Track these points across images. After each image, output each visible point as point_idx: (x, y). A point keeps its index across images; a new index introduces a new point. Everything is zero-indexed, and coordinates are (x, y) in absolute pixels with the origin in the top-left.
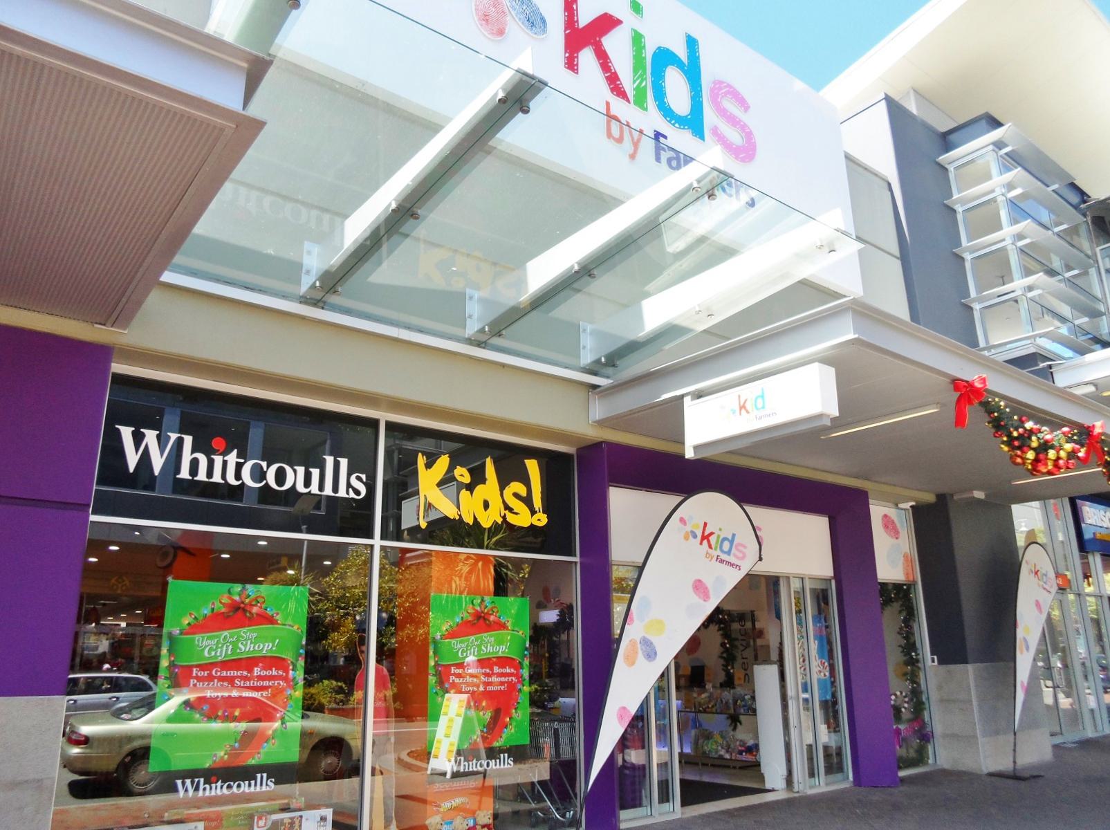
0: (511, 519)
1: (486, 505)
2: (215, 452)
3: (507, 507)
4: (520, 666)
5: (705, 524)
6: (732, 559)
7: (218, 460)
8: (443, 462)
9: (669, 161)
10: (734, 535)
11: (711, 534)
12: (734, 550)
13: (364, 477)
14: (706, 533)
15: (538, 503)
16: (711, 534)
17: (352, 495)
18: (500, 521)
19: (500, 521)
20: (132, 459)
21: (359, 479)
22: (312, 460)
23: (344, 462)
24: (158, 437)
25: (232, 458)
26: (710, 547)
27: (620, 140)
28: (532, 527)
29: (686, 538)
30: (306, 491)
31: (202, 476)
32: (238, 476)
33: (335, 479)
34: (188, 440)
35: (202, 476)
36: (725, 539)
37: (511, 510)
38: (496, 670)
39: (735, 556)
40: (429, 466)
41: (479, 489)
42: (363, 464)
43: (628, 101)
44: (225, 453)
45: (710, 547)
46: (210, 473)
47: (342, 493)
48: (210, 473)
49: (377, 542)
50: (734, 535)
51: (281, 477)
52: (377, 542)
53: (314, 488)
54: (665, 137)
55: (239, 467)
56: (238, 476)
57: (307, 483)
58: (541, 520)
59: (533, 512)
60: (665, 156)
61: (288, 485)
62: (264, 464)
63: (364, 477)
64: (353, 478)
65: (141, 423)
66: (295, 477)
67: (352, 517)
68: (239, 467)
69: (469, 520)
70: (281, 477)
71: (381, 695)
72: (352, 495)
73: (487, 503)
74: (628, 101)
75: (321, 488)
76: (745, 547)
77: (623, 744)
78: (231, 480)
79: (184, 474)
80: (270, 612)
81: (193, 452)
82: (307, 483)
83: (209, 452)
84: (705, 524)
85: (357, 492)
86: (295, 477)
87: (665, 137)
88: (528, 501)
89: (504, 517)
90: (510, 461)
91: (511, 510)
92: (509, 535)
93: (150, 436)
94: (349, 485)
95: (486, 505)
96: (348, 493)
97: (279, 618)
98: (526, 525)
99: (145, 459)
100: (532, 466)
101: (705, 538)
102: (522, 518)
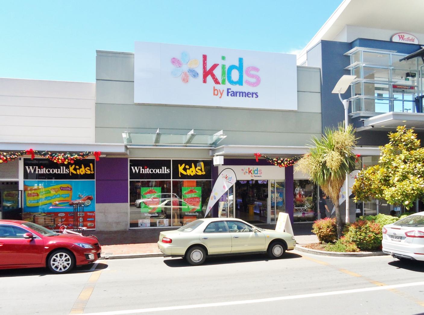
0: (197, 174)
1: (192, 172)
3: (197, 172)
4: (200, 198)
5: (205, 57)
6: (245, 88)
7: (146, 170)
8: (184, 165)
9: (231, 95)
10: (241, 60)
11: (215, 66)
12: (245, 77)
14: (208, 68)
15: (203, 170)
16: (215, 66)
17: (167, 173)
18: (195, 174)
19: (195, 174)
20: (28, 171)
21: (67, 170)
22: (160, 168)
23: (165, 167)
25: (148, 169)
26: (217, 82)
27: (217, 95)
28: (202, 175)
29: (185, 80)
31: (144, 172)
33: (164, 170)
34: (141, 167)
35: (144, 172)
36: (232, 67)
37: (197, 172)
38: (195, 199)
39: (248, 83)
40: (181, 166)
41: (191, 169)
42: (168, 167)
44: (147, 169)
45: (217, 82)
47: (165, 173)
49: (172, 180)
50: (241, 60)
51: (155, 171)
52: (172, 180)
53: (161, 172)
54: (230, 89)
55: (149, 170)
56: (149, 172)
58: (204, 173)
59: (202, 172)
60: (230, 94)
61: (156, 172)
62: (50, 169)
63: (169, 169)
64: (167, 170)
65: (134, 166)
66: (158, 171)
67: (168, 176)
68: (149, 170)
69: (189, 175)
70: (155, 171)
73: (192, 171)
76: (257, 70)
77: (347, 151)
79: (141, 172)
80: (155, 191)
83: (144, 169)
84: (205, 57)
86: (158, 171)
87: (230, 89)
88: (201, 170)
89: (196, 173)
90: (196, 162)
91: (197, 172)
92: (196, 176)
93: (136, 168)
94: (167, 171)
95: (192, 172)
97: (157, 192)
98: (201, 174)
99: (136, 171)
100: (202, 164)
101: (208, 73)
102: (200, 173)
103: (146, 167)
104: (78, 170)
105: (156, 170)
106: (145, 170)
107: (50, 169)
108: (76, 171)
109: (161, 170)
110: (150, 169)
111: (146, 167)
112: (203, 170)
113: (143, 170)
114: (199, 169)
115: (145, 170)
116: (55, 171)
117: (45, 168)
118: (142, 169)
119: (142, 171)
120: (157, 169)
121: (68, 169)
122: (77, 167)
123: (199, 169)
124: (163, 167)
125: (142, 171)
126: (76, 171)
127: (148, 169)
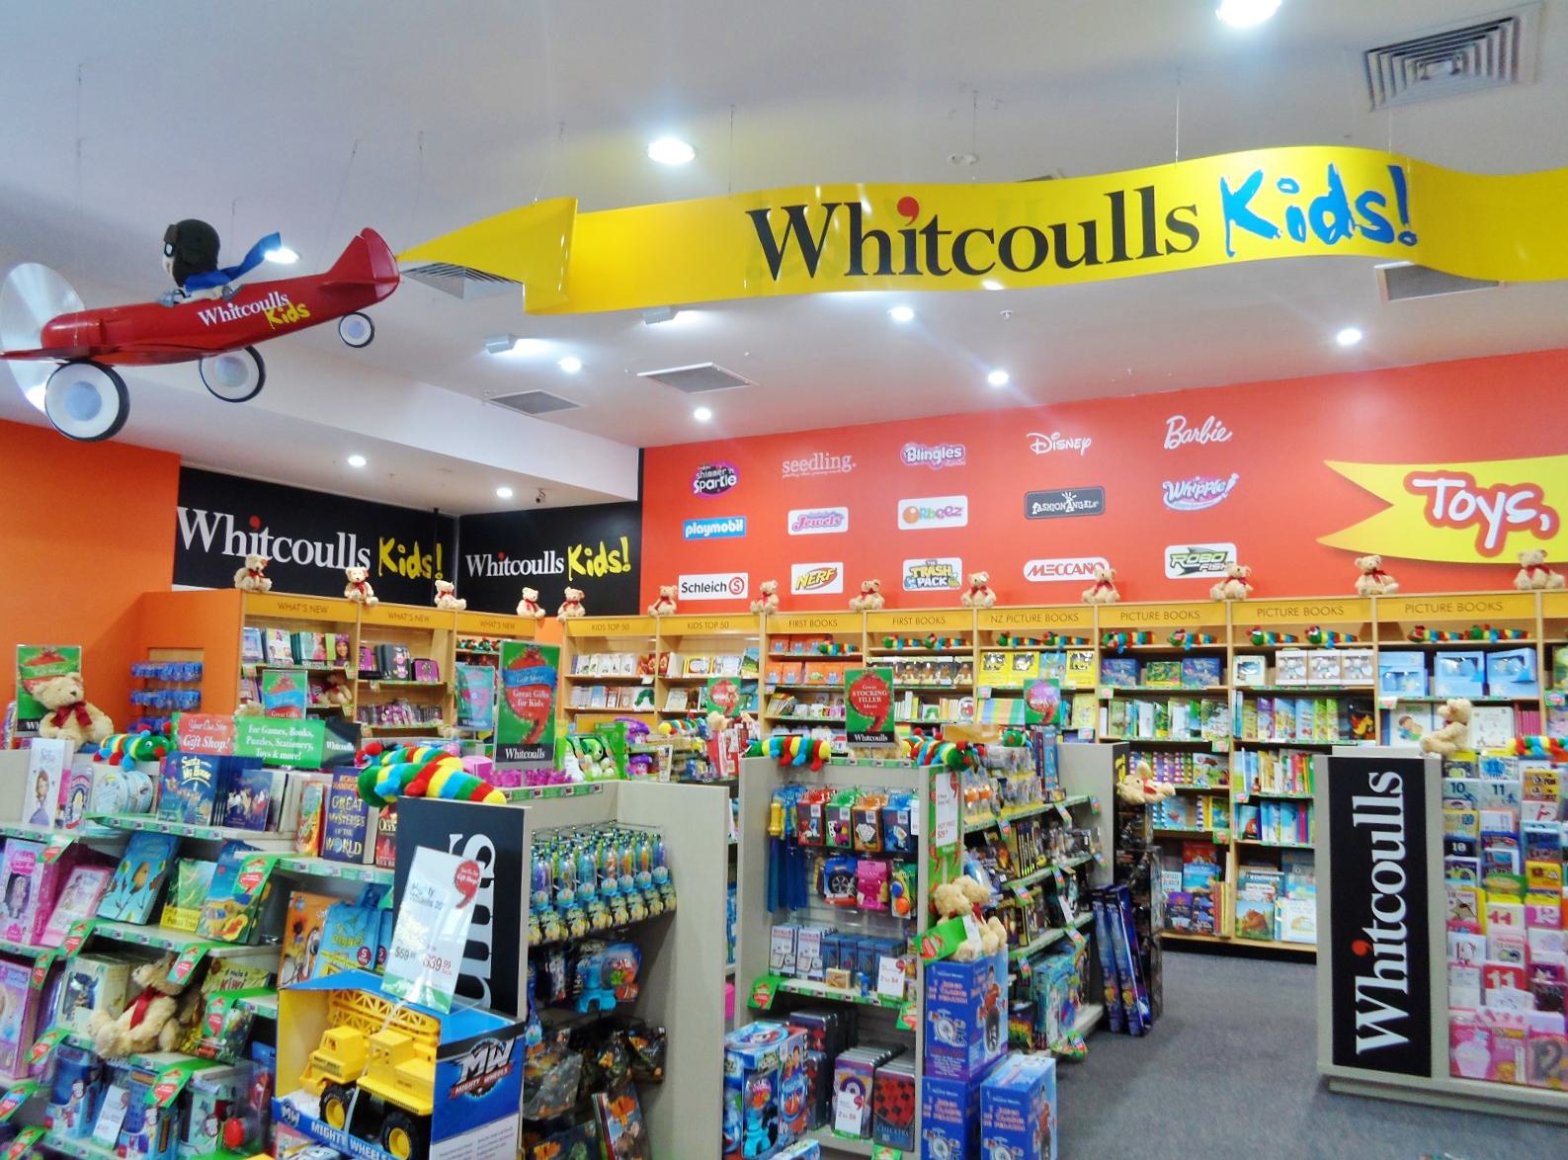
0: (612, 570)
2: (1370, 951)
13: (1372, 775)
15: (626, 559)
17: (1399, 790)
20: (1392, 1039)
21: (1376, 781)
24: (1362, 1011)
30: (1401, 846)
31: (1402, 966)
32: (1395, 926)
34: (230, 519)
35: (1402, 966)
43: (993, 242)
44: (260, 531)
46: (1398, 958)
48: (1398, 958)
51: (1388, 878)
53: (329, 563)
55: (1383, 925)
56: (1395, 926)
57: (324, 558)
59: (623, 564)
61: (308, 561)
62: (1375, 897)
63: (368, 551)
64: (1376, 789)
68: (1383, 925)
70: (1388, 878)
71: (1345, 710)
72: (1399, 790)
74: (993, 242)
75: (1395, 828)
78: (1402, 933)
81: (1374, 976)
82: (324, 558)
83: (247, 530)
85: (1394, 783)
88: (620, 559)
93: (477, 557)
94: (1386, 794)
96: (1397, 795)
103: (254, 521)
104: (284, 316)
105: (1377, 869)
106: (249, 540)
107: (1375, 897)
108: (281, 318)
109: (330, 547)
110: (275, 533)
111: (254, 521)
112: (626, 559)
113: (1379, 966)
114: (615, 557)
115: (249, 540)
116: (1386, 861)
117: (270, 534)
118: (1372, 975)
119: (1388, 974)
120: (1373, 865)
121: (1372, 775)
122: (402, 549)
123: (615, 557)
124: (342, 536)
125: (1388, 974)
126: (281, 318)
127: (1374, 933)
